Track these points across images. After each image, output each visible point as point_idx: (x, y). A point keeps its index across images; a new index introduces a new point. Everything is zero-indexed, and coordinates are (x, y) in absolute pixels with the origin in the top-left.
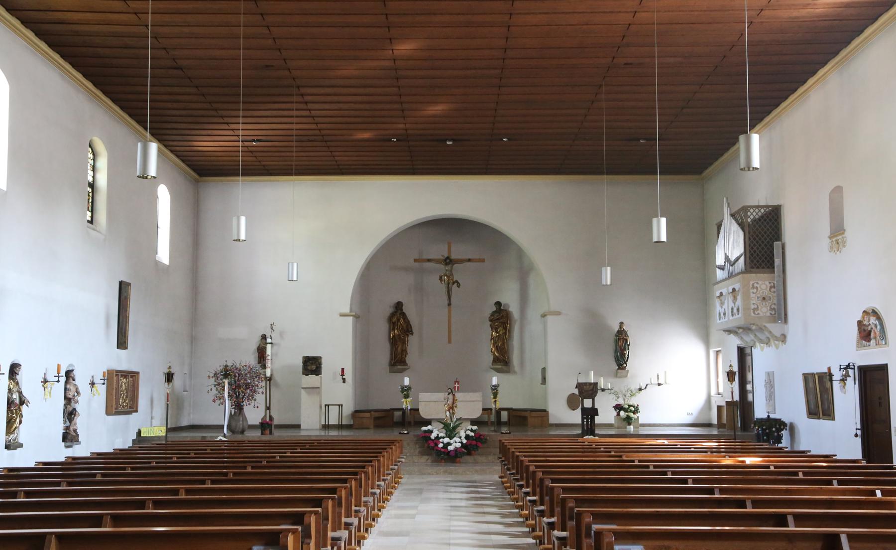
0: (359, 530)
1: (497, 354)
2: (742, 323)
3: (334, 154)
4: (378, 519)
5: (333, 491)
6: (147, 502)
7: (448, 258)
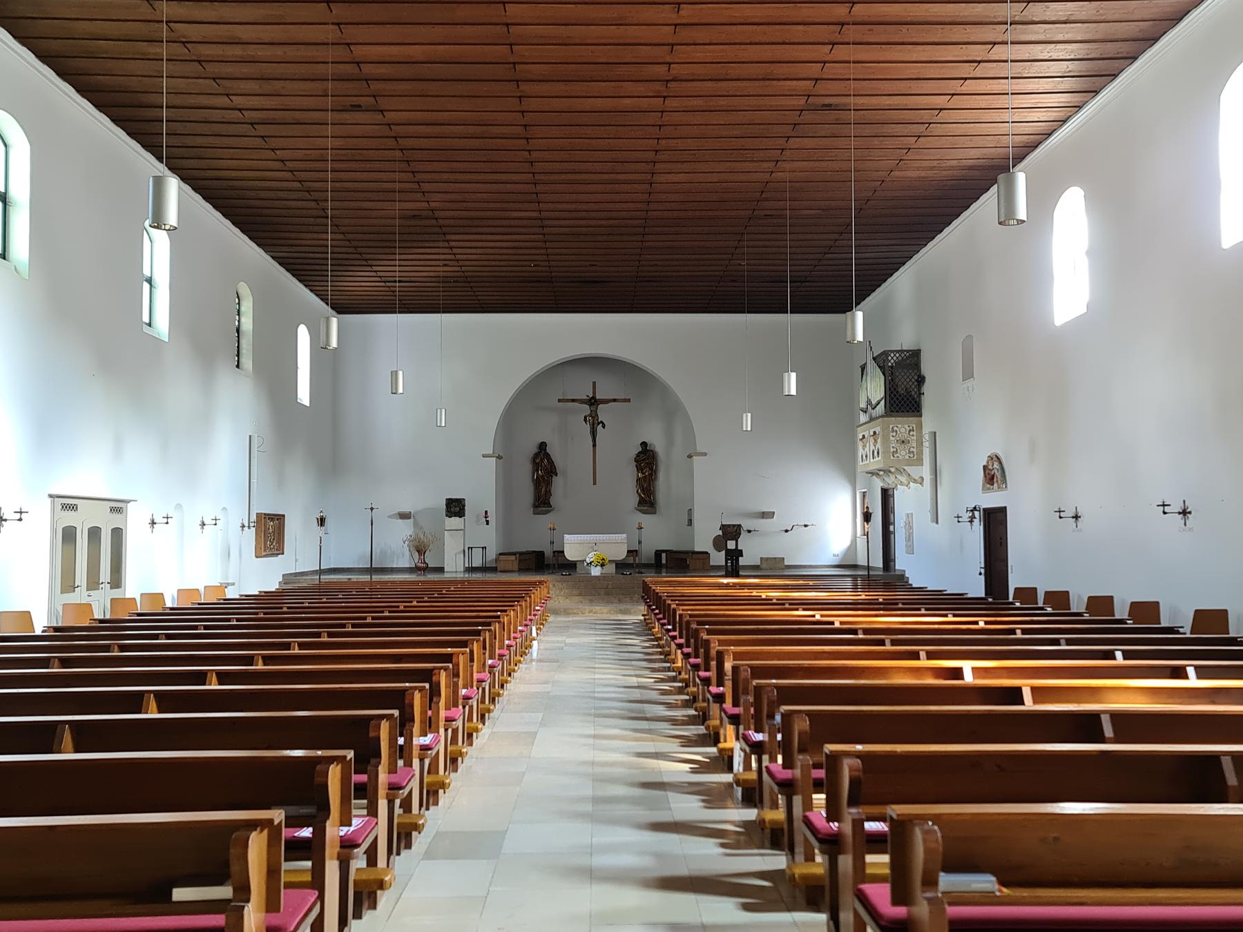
0: (503, 675)
1: (643, 496)
2: (881, 466)
3: (419, 177)
4: (500, 698)
5: (448, 658)
6: (292, 644)
7: (594, 398)
